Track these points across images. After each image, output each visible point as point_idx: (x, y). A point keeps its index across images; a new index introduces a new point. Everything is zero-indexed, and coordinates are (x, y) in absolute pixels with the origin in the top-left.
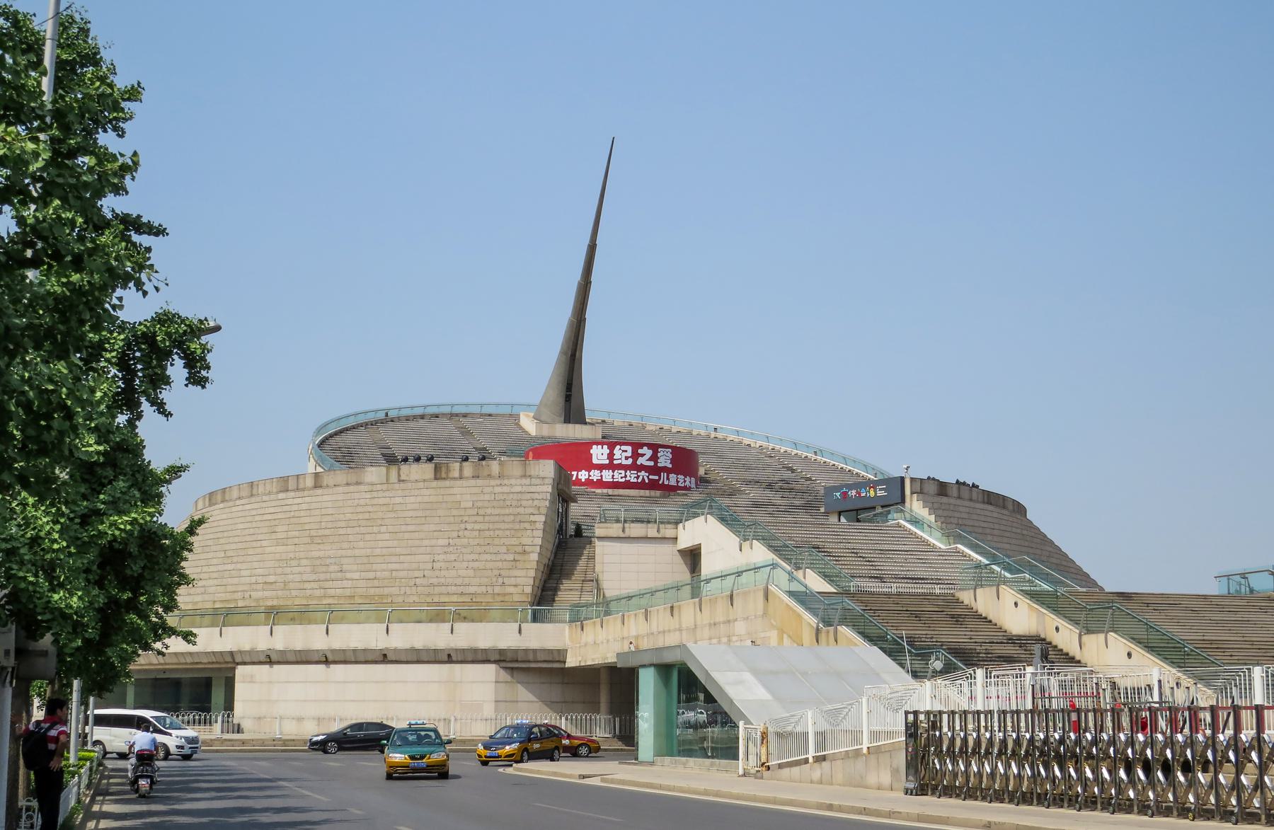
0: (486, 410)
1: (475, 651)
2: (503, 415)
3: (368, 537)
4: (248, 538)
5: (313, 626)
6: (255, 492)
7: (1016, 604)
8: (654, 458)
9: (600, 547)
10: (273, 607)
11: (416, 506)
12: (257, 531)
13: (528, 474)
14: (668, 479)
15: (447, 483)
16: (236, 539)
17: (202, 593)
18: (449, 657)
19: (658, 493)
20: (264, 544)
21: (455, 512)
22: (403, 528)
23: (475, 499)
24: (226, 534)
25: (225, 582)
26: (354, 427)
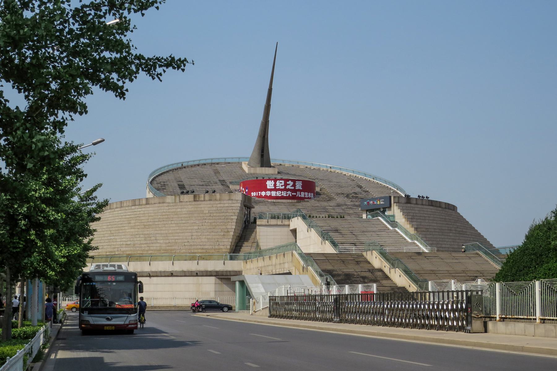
0: (228, 161)
1: (207, 271)
2: (235, 163)
3: (166, 225)
4: (120, 226)
5: (145, 262)
6: (122, 205)
7: (376, 258)
8: (294, 185)
9: (258, 229)
10: (129, 254)
11: (186, 212)
12: (123, 222)
13: (231, 199)
14: (300, 194)
15: (199, 203)
16: (115, 226)
17: (102, 249)
18: (197, 274)
19: (295, 201)
20: (126, 228)
21: (201, 215)
22: (181, 222)
23: (209, 209)
24: (111, 224)
25: (110, 244)
26: (167, 172)
